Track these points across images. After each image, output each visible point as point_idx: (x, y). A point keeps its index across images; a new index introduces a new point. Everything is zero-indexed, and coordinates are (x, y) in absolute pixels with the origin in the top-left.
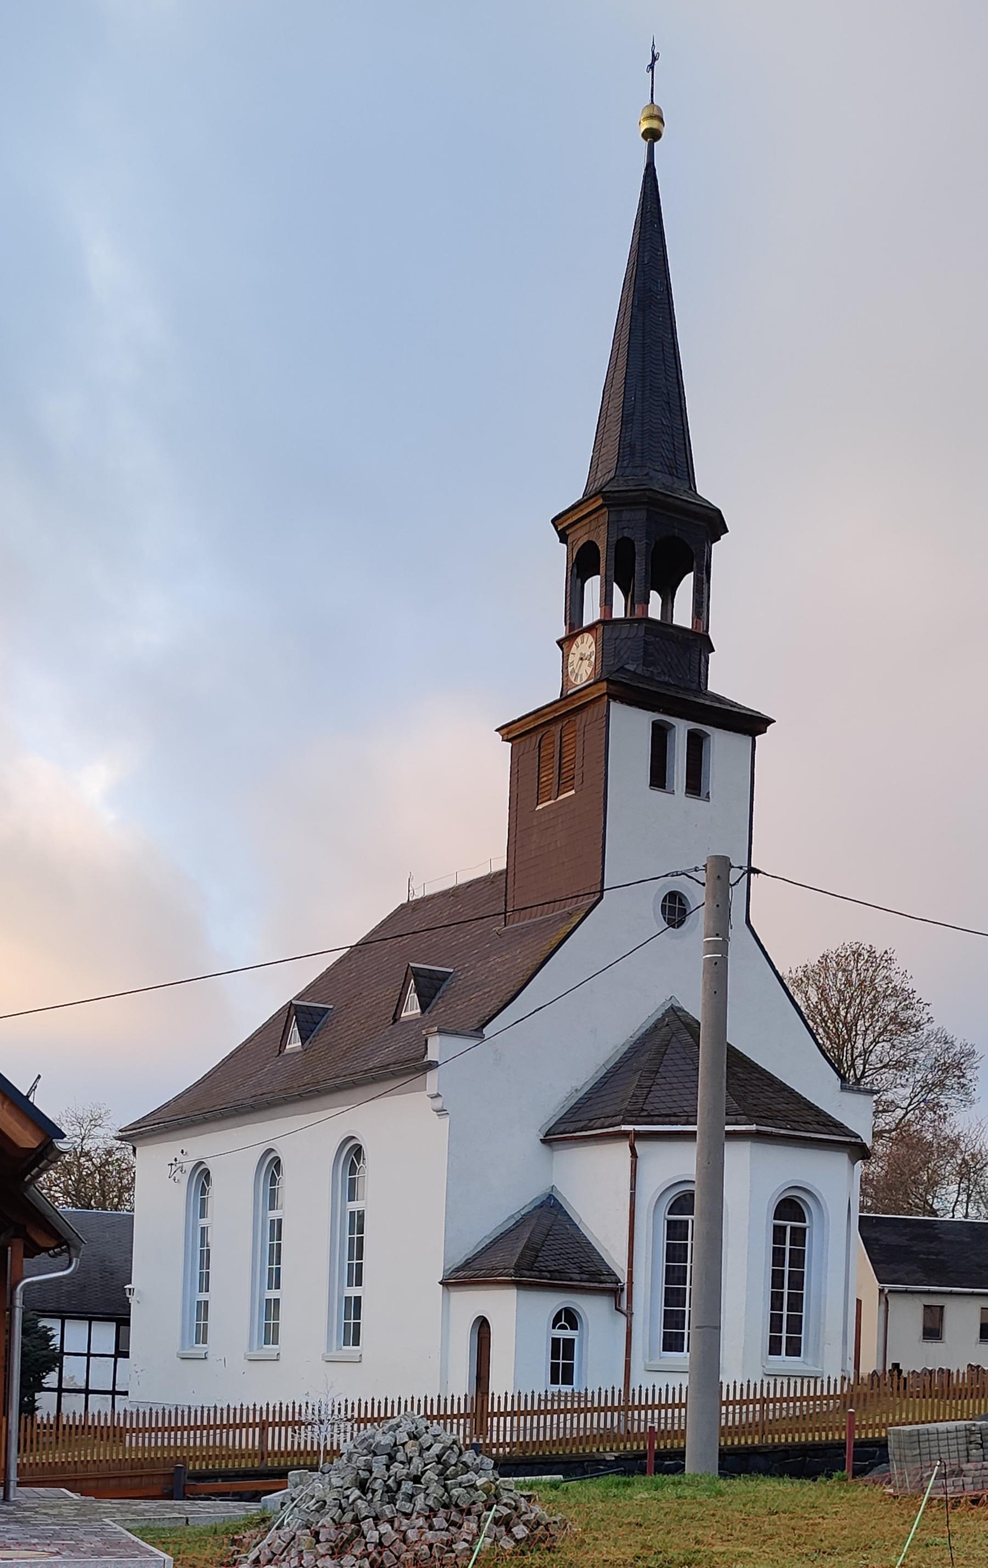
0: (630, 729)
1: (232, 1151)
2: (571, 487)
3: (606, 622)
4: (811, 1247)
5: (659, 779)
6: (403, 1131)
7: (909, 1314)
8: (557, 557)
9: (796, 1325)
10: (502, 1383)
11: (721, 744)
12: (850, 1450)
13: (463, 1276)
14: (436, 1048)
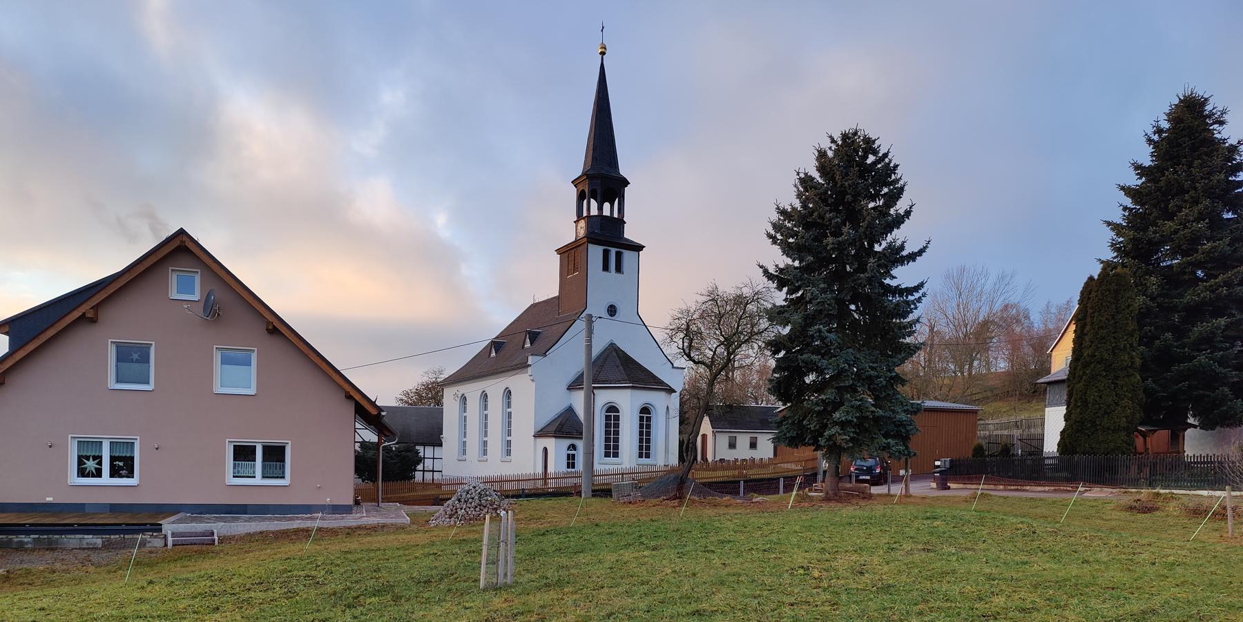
0: (596, 252)
1: (472, 390)
2: (578, 171)
3: (589, 216)
4: (653, 423)
5: (606, 268)
6: (521, 385)
7: (723, 440)
8: (573, 192)
9: (648, 448)
10: (551, 469)
11: (628, 255)
12: (890, 480)
13: (540, 434)
14: (531, 360)
